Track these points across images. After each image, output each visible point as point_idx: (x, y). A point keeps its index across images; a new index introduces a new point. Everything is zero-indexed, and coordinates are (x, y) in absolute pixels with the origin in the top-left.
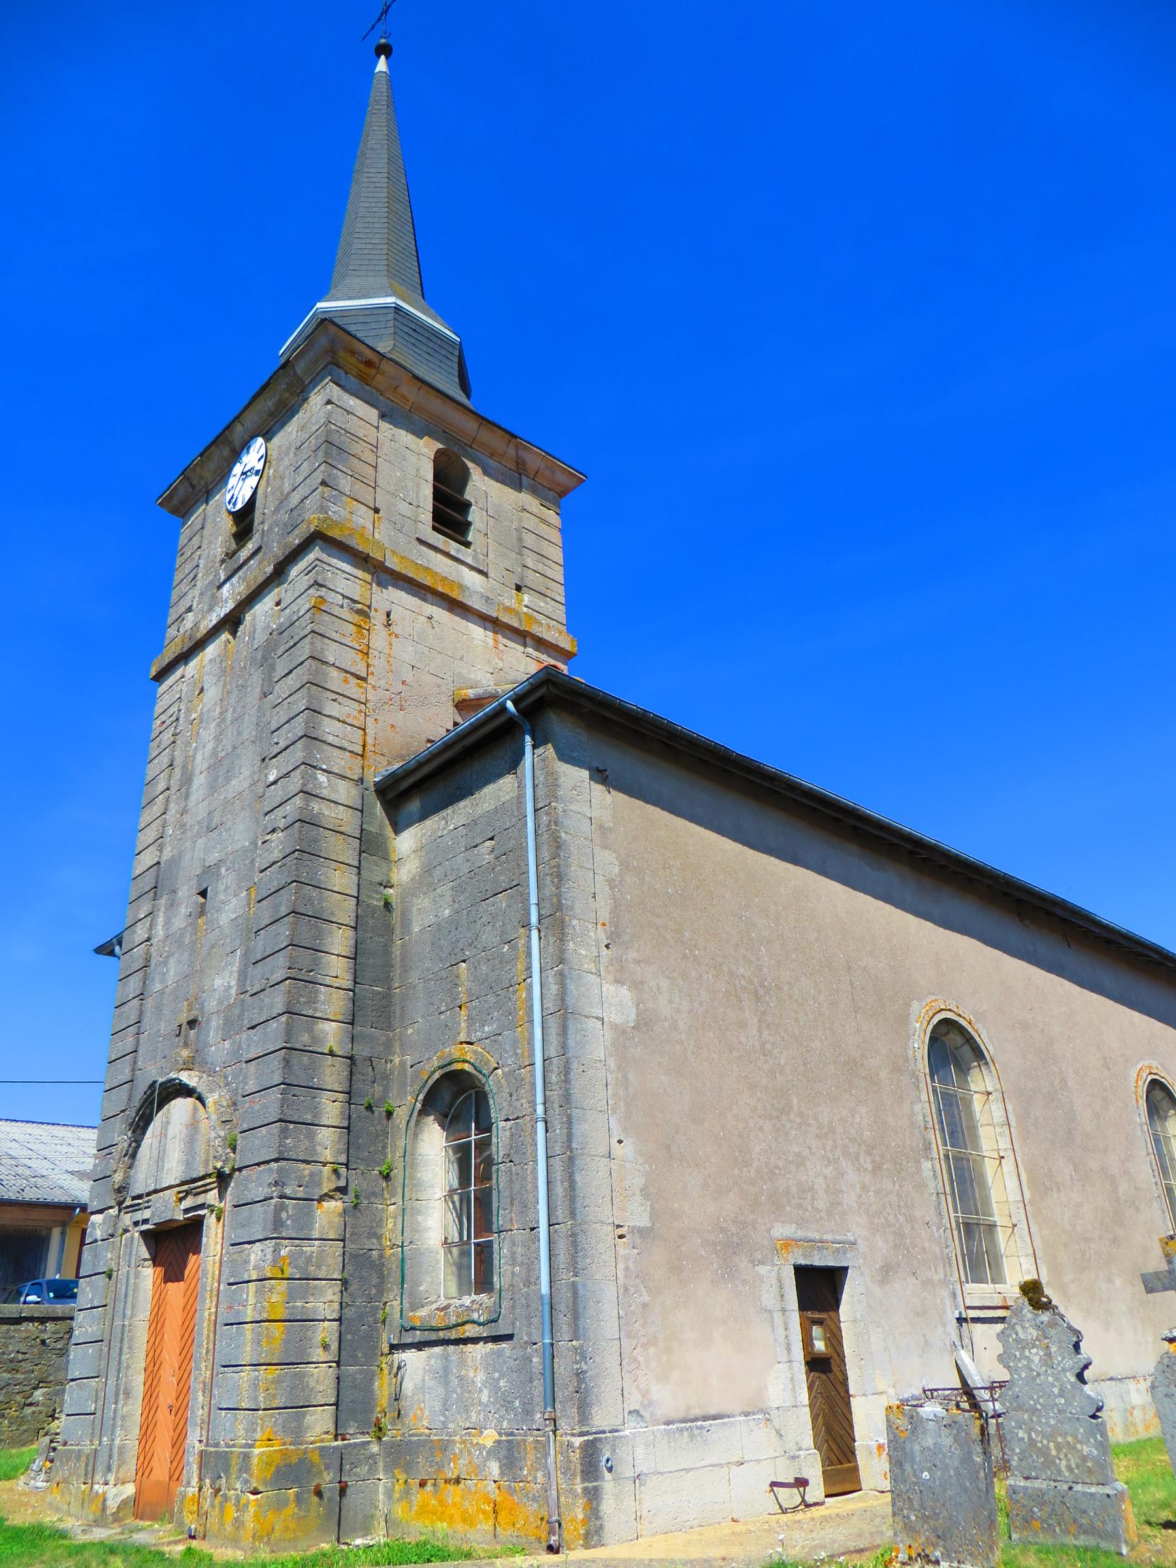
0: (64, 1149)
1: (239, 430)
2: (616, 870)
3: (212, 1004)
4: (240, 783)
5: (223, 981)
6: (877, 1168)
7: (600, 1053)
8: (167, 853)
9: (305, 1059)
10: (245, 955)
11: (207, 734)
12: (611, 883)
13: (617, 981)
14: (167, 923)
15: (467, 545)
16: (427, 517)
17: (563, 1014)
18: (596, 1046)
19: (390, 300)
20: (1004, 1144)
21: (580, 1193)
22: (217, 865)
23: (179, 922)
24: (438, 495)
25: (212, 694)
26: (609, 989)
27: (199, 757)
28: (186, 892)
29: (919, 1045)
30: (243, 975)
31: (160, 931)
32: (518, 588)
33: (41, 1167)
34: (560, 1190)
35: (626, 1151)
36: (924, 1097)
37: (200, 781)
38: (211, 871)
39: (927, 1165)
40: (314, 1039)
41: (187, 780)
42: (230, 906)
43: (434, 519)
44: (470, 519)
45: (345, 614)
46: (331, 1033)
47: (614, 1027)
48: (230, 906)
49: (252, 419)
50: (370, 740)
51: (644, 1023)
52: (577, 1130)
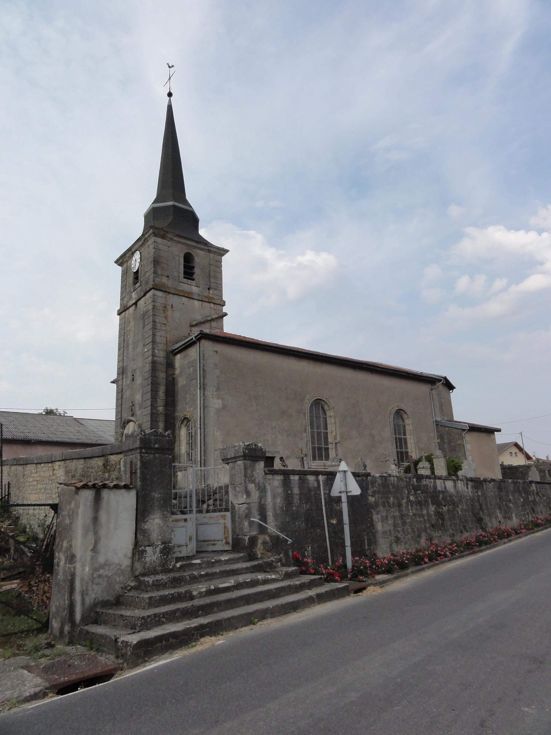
0: (108, 428)
1: (133, 250)
2: (219, 374)
3: (136, 402)
4: (139, 349)
5: (138, 398)
6: (288, 436)
7: (213, 415)
8: (125, 364)
9: (155, 415)
10: (143, 391)
11: (132, 334)
12: (217, 377)
13: (218, 399)
14: (126, 381)
15: (193, 280)
16: (182, 275)
17: (204, 407)
18: (212, 412)
19: (171, 203)
20: (333, 429)
21: (206, 442)
22: (136, 369)
23: (129, 382)
24: (185, 267)
25: (132, 323)
26: (215, 401)
27: (130, 340)
28: (129, 375)
29: (307, 406)
30: (142, 396)
31: (124, 383)
32: (209, 289)
33: (101, 434)
34: (202, 441)
35: (219, 433)
36: (306, 418)
37: (131, 347)
38: (134, 371)
39: (304, 434)
40: (157, 411)
41: (128, 346)
42: (139, 380)
43: (184, 274)
44: (194, 271)
45: (161, 308)
46: (161, 409)
47: (216, 408)
48: (139, 380)
49: (136, 247)
50: (168, 340)
51: (224, 407)
52: (206, 430)
